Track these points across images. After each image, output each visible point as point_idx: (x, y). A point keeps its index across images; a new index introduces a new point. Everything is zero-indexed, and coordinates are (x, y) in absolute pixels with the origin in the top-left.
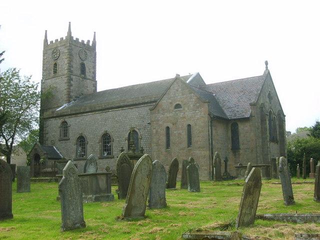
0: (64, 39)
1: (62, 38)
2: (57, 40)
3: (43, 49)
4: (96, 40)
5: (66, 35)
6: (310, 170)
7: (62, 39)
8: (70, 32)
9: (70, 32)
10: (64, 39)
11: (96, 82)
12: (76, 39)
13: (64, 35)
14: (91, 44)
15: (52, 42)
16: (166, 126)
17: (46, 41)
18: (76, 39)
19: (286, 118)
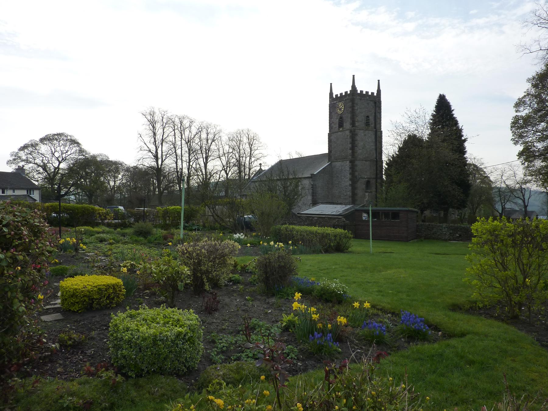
0: (349, 92)
1: (342, 93)
2: (341, 94)
3: (329, 103)
4: (381, 89)
5: (351, 89)
6: (186, 192)
7: (346, 92)
8: (354, 87)
9: (354, 87)
10: (349, 92)
11: (382, 131)
12: (361, 91)
13: (349, 89)
14: (375, 94)
15: (337, 95)
16: (259, 163)
17: (331, 94)
18: (361, 91)
19: (285, 157)
